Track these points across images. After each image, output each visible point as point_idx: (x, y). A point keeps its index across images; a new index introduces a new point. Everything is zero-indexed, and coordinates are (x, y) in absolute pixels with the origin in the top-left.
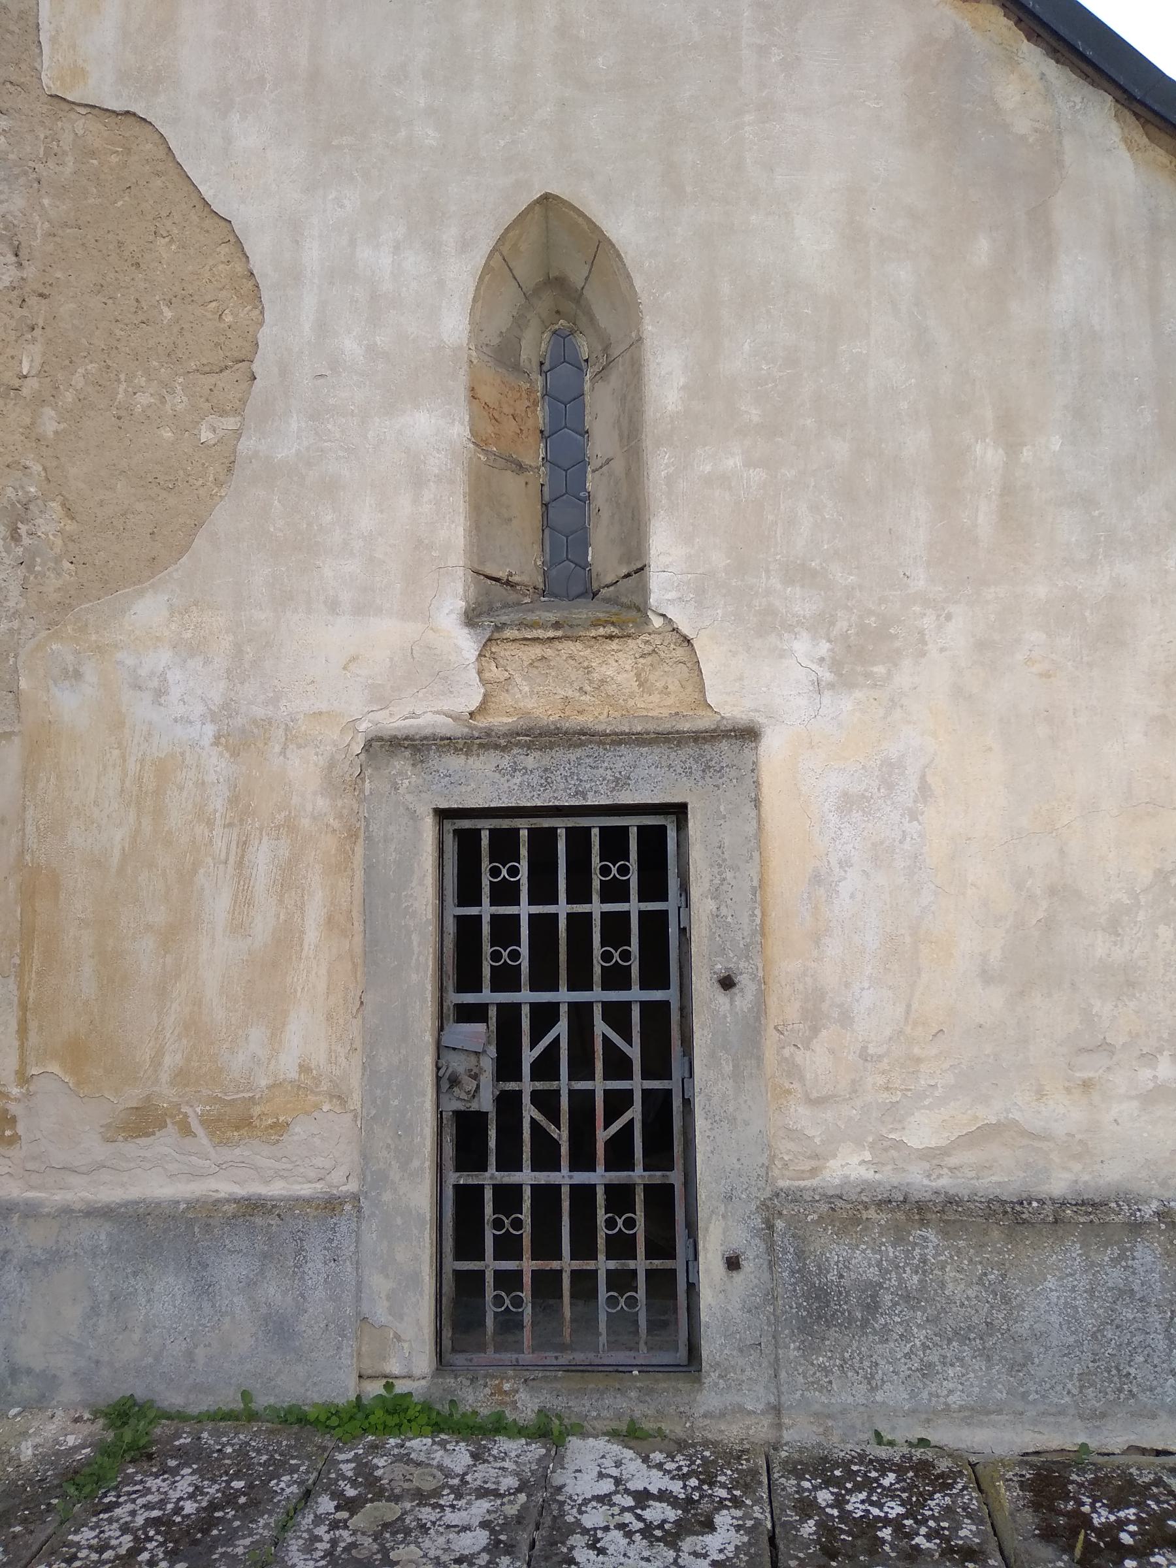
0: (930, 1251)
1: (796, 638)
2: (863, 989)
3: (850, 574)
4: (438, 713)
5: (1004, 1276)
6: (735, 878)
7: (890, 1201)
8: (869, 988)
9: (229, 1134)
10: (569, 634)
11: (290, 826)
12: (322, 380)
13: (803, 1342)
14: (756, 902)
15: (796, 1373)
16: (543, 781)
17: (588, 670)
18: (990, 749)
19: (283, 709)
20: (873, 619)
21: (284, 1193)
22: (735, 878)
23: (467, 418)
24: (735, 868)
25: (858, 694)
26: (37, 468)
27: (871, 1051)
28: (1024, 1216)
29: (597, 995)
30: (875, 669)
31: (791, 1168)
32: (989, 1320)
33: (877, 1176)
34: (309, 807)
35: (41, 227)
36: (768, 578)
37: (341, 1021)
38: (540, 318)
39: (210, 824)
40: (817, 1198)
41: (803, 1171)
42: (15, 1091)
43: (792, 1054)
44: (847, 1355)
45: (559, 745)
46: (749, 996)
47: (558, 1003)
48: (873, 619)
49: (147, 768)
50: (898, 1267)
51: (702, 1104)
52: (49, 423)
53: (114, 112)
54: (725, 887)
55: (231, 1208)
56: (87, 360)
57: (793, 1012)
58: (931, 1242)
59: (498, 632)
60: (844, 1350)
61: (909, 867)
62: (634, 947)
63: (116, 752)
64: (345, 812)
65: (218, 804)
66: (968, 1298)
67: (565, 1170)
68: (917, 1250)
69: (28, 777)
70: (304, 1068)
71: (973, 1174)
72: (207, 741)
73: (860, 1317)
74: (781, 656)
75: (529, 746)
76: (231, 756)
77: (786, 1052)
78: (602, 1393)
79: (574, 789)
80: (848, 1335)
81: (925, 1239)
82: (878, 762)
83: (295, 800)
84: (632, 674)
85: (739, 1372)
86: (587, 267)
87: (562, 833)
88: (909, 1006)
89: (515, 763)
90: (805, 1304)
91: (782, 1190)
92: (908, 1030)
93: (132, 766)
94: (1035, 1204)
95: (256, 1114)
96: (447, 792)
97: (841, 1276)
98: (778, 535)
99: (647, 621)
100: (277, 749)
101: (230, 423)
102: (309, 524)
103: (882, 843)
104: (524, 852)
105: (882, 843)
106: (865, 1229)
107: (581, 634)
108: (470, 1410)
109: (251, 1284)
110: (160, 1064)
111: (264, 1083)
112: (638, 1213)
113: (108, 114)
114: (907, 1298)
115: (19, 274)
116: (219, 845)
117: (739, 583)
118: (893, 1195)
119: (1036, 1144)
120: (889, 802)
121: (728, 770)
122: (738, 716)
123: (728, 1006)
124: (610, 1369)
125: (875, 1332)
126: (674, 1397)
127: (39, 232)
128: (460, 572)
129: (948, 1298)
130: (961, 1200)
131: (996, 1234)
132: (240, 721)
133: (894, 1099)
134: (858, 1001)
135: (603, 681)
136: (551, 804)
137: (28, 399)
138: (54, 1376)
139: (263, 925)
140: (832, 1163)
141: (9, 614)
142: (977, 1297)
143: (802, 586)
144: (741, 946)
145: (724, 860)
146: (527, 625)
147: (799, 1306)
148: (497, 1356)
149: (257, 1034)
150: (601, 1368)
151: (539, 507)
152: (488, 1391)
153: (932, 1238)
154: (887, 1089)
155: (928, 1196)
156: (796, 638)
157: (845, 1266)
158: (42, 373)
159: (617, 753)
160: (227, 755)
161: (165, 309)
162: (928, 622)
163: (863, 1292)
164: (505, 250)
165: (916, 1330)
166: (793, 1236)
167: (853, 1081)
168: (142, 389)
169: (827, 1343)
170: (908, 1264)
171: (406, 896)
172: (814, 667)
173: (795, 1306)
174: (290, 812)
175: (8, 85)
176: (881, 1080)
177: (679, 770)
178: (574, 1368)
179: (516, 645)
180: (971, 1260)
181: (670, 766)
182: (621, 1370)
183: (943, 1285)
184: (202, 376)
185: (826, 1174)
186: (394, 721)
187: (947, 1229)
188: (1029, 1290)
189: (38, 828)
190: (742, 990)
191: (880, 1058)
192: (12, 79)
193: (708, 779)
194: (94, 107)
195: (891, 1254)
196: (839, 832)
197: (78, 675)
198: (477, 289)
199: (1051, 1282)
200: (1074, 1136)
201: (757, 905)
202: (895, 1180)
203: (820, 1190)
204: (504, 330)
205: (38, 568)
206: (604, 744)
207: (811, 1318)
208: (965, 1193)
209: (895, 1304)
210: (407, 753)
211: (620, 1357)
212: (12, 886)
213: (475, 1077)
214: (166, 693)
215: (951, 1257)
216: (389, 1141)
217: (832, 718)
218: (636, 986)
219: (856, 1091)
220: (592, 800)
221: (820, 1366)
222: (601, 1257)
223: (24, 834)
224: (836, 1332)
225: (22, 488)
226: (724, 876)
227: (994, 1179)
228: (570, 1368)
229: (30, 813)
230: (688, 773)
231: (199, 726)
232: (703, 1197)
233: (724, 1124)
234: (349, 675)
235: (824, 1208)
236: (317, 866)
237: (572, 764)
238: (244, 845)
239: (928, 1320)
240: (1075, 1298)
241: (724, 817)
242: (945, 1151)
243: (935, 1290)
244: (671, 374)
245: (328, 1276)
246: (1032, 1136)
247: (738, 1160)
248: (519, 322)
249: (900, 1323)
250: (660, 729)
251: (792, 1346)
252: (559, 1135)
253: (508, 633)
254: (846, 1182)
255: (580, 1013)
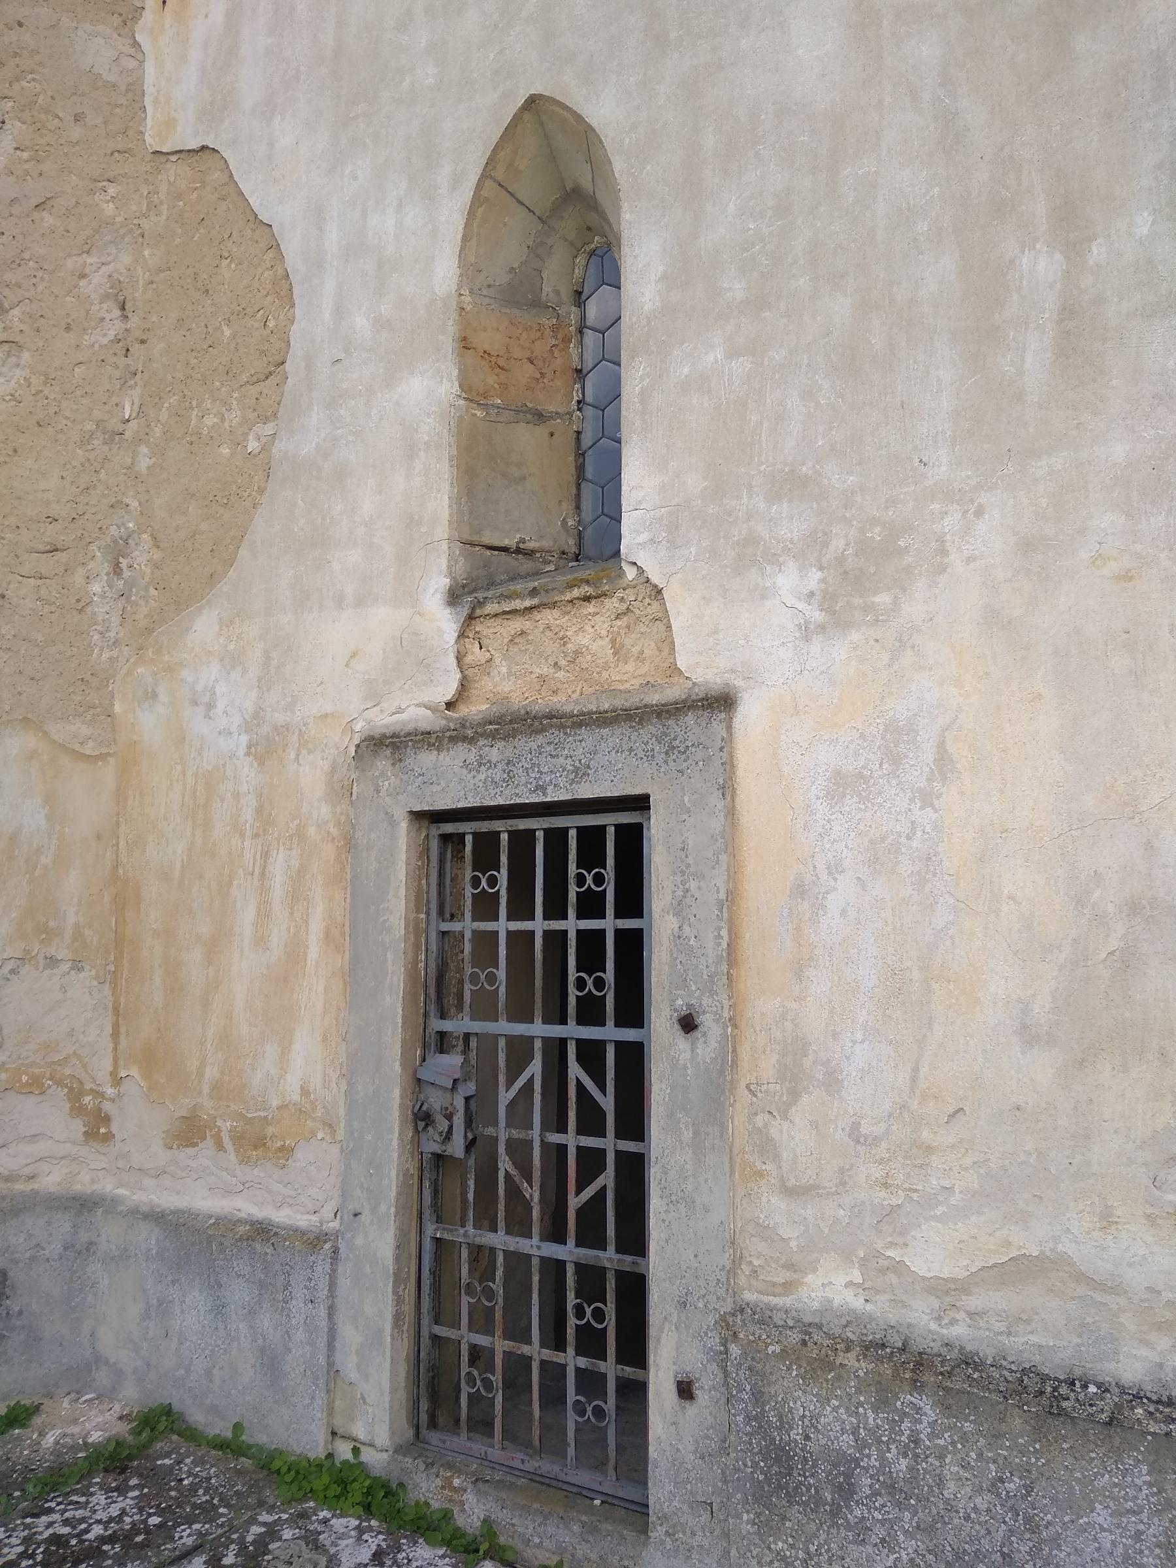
0: (924, 1429)
1: (780, 571)
2: (854, 1042)
3: (850, 473)
4: (418, 705)
5: (1029, 1489)
6: (699, 888)
7: (883, 1346)
8: (863, 1042)
9: (249, 1152)
10: (545, 600)
11: (300, 835)
12: (339, 366)
13: (758, 1515)
14: (721, 920)
15: (749, 1554)
16: (505, 776)
17: (564, 641)
18: (1040, 697)
19: (298, 713)
20: (877, 530)
21: (287, 1221)
22: (699, 888)
23: (455, 372)
24: (700, 876)
25: (855, 636)
26: (134, 504)
27: (865, 1129)
28: (1065, 1404)
29: (573, 1030)
30: (877, 599)
31: (761, 1277)
32: (1005, 1550)
33: (869, 1307)
34: (315, 815)
35: (143, 277)
36: (750, 497)
37: (333, 1043)
38: (566, 240)
39: (242, 835)
40: (790, 1323)
41: (774, 1284)
42: (110, 1091)
43: (766, 1125)
44: (813, 1548)
45: (521, 733)
46: (713, 1044)
47: (533, 1037)
48: (877, 530)
49: (199, 780)
50: (879, 1442)
51: (658, 1177)
52: (144, 463)
53: (194, 150)
54: (688, 901)
55: (242, 1229)
56: (171, 394)
57: (768, 1067)
58: (926, 1414)
59: (481, 608)
60: (809, 1541)
61: (919, 872)
62: (609, 975)
63: (179, 767)
64: (343, 819)
65: (248, 815)
66: (975, 1509)
67: (535, 1240)
68: (906, 1425)
69: (120, 795)
70: (305, 1092)
71: (1001, 1327)
72: (241, 752)
73: (829, 1499)
74: (763, 597)
75: (493, 736)
76: (259, 765)
77: (760, 1120)
78: (546, 1518)
79: (534, 783)
80: (814, 1520)
81: (918, 1410)
82: (881, 727)
83: (305, 808)
84: (608, 639)
85: (688, 1533)
86: (589, 164)
87: (540, 835)
88: (916, 1070)
89: (481, 756)
90: (762, 1464)
91: (748, 1304)
92: (914, 1104)
93: (190, 780)
94: (1092, 1389)
95: (269, 1135)
96: (419, 793)
97: (807, 1438)
98: (764, 439)
99: (621, 574)
100: (293, 756)
101: (269, 429)
102: (324, 519)
103: (883, 839)
104: (504, 859)
105: (883, 839)
106: (838, 1378)
107: (556, 598)
108: (423, 1499)
109: (252, 1313)
110: (203, 1076)
111: (275, 1102)
112: (609, 1304)
113: (191, 154)
114: (891, 1488)
115: (124, 326)
116: (248, 855)
117: (717, 509)
118: (889, 1338)
119: (1098, 1297)
120: (894, 782)
121: (694, 750)
122: (712, 681)
123: (688, 1055)
124: (574, 1490)
125: (848, 1527)
126: (619, 1544)
127: (141, 282)
128: (445, 546)
129: (947, 1502)
130: (983, 1363)
131: (1017, 1423)
132: (265, 729)
133: (895, 1201)
134: (848, 1058)
135: (577, 653)
136: (512, 802)
137: (130, 441)
138: (121, 1370)
139: (277, 938)
140: (810, 1279)
141: (110, 643)
142: (988, 1510)
143: (790, 501)
144: (705, 977)
145: (688, 866)
146: (506, 597)
147: (755, 1465)
148: (468, 1444)
149: (271, 1050)
150: (565, 1487)
151: (572, 458)
152: (439, 1482)
153: (927, 1409)
154: (886, 1185)
155: (936, 1347)
156: (780, 571)
157: (812, 1425)
158: (141, 413)
159: (577, 738)
160: (256, 765)
161: (225, 328)
162: (951, 523)
163: (835, 1466)
164: (499, 174)
165: (902, 1538)
166: (750, 1369)
167: (842, 1170)
168: (208, 412)
169: (788, 1524)
170: (894, 1441)
171: (383, 909)
172: (801, 605)
173: (749, 1464)
174: (300, 820)
175: (116, 154)
176: (877, 1173)
177: (641, 754)
178: (538, 1478)
179: (499, 620)
180: (980, 1455)
181: (631, 750)
182: (583, 1494)
183: (941, 1482)
184: (252, 387)
185: (803, 1292)
186: (384, 719)
187: (948, 1401)
188: (1066, 1519)
189: (127, 843)
190: (704, 1035)
191: (876, 1140)
192: (119, 147)
193: (672, 764)
194: (181, 151)
195: (871, 1421)
196: (828, 827)
197: (155, 696)
198: (467, 226)
199: (1101, 1516)
200: (1159, 1292)
201: (723, 924)
202: (893, 1317)
203: (794, 1314)
204: (516, 265)
205: (133, 598)
206: (565, 727)
207: (769, 1486)
208: (988, 1353)
209: (876, 1494)
210: (388, 752)
211: (585, 1478)
212: (107, 898)
213: (449, 1117)
214: (215, 706)
215: (953, 1443)
216: (363, 1180)
217: (822, 672)
218: (610, 1022)
219: (844, 1184)
220: (552, 796)
221: (778, 1554)
222: (571, 1351)
223: (118, 850)
224: (799, 1512)
225: (124, 524)
226: (687, 886)
227: (1033, 1339)
228: (534, 1477)
229: (123, 828)
230: (650, 756)
231: (236, 737)
232: (656, 1297)
233: (682, 1206)
234: (350, 671)
235: (795, 1337)
236: (319, 877)
237: (533, 754)
238: (266, 855)
239: (918, 1527)
240: (1141, 1552)
241: (688, 811)
242: (962, 1287)
243: (930, 1487)
244: (649, 264)
245: (307, 1317)
246: (1101, 1286)
247: (696, 1256)
248: (538, 251)
249: (883, 1522)
250: (627, 705)
251: (745, 1517)
252: (531, 1196)
253: (491, 608)
254: (827, 1307)
255: (557, 1049)
